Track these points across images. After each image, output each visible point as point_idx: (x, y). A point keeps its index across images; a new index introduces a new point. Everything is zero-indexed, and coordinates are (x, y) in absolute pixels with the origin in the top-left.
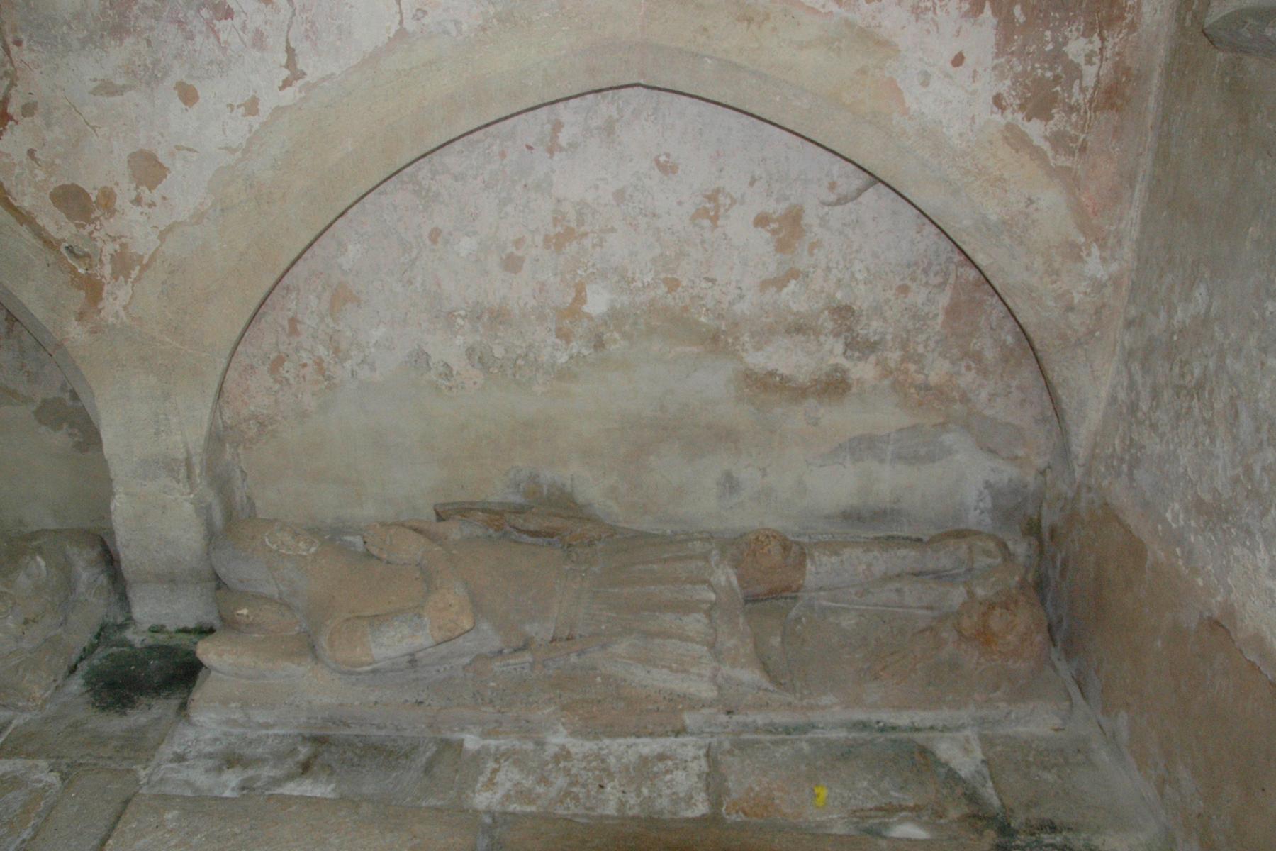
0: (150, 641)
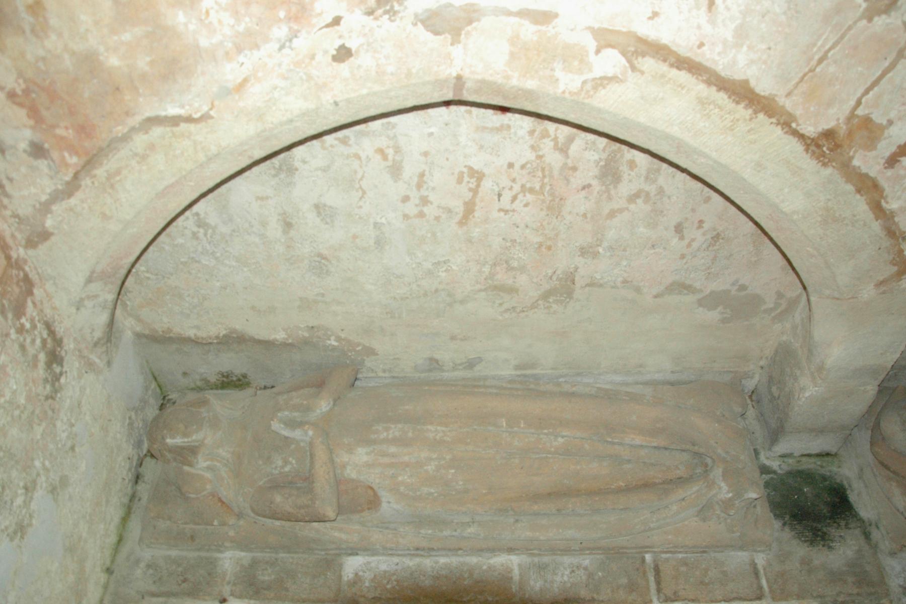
0: (786, 468)
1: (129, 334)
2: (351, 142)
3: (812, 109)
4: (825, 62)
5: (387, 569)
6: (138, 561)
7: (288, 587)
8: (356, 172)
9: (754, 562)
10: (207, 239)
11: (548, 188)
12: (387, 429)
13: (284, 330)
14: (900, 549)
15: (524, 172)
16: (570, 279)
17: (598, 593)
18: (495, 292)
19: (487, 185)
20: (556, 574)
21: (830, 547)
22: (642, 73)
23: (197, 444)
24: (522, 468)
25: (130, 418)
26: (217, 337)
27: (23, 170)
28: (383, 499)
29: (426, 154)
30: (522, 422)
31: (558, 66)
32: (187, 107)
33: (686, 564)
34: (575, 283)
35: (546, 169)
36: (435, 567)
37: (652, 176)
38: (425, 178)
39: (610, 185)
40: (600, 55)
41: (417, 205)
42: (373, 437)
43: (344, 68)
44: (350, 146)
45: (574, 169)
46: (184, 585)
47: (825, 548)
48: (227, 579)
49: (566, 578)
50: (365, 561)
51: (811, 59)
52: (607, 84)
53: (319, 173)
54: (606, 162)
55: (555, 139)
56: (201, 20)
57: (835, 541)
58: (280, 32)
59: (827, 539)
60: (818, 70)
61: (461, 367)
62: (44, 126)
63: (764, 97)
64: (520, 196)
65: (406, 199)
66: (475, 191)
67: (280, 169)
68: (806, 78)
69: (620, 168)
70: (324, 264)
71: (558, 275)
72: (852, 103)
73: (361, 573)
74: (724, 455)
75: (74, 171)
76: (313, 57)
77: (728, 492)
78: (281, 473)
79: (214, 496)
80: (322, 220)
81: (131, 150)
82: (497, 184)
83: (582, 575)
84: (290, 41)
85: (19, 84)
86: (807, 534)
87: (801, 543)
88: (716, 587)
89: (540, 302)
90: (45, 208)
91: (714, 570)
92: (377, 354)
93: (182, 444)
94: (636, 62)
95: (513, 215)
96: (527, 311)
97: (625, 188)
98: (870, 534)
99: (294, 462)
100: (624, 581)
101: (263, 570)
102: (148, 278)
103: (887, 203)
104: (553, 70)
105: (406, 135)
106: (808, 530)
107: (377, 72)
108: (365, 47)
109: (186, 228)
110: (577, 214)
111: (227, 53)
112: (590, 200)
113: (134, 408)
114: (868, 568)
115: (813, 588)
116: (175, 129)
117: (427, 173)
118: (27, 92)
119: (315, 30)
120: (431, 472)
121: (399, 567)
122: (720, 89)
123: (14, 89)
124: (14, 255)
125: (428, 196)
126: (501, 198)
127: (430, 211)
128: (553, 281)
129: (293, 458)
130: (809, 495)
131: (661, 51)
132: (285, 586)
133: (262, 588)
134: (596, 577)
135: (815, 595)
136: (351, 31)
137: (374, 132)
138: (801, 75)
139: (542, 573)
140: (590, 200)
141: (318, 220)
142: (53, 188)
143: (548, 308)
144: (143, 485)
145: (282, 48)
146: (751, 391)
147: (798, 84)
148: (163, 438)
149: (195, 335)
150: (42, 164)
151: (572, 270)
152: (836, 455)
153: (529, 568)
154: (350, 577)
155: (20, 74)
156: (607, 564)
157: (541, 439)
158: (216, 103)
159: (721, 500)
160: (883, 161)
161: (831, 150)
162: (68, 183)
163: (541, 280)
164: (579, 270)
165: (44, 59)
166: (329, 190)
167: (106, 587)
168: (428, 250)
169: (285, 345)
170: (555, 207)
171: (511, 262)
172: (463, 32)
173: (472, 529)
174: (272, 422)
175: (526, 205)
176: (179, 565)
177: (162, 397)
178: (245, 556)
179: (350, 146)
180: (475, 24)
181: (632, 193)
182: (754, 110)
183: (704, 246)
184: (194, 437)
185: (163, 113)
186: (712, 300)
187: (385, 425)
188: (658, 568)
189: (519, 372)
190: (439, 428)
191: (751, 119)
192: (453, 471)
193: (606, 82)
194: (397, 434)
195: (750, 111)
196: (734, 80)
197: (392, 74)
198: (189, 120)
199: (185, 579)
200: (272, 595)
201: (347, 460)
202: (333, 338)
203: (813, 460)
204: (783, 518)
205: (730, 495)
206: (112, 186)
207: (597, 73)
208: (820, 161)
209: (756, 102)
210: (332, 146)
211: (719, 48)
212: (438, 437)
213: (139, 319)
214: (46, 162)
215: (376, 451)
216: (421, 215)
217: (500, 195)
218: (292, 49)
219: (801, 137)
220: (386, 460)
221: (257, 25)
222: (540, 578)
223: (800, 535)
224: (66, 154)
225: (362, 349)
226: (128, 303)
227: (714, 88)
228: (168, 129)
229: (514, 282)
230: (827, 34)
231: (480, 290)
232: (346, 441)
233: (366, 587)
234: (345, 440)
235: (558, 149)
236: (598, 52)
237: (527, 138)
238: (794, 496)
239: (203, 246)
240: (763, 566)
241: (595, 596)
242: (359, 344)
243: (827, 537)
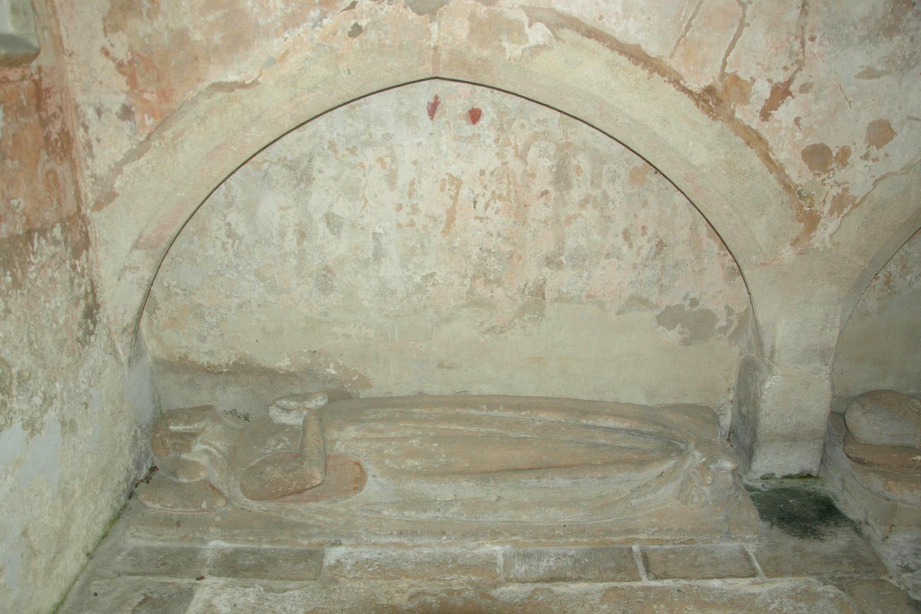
1: (149, 359)
2: (357, 152)
3: (692, 68)
4: (691, 29)
5: (369, 557)
8: (360, 180)
10: (234, 250)
11: (513, 194)
14: (889, 530)
15: (494, 178)
16: (539, 292)
18: (476, 308)
19: (465, 191)
22: (564, 41)
23: (196, 432)
26: (227, 365)
27: (111, 130)
28: (370, 473)
29: (415, 163)
31: (504, 37)
32: (243, 74)
34: (545, 298)
35: (510, 176)
37: (596, 181)
38: (415, 187)
39: (563, 191)
40: (532, 27)
41: (408, 214)
42: (362, 418)
43: (356, 42)
44: (357, 155)
45: (533, 175)
48: (208, 563)
51: (681, 27)
52: (540, 51)
53: (331, 181)
54: (557, 169)
55: (515, 147)
56: (262, 5)
58: (314, 14)
60: (687, 35)
62: (136, 92)
63: (654, 59)
64: (491, 203)
65: (399, 207)
66: (455, 198)
67: (301, 179)
68: (681, 42)
69: (570, 174)
70: (329, 279)
71: (530, 288)
72: (720, 63)
75: (149, 132)
76: (335, 34)
77: (702, 458)
80: (330, 230)
81: (195, 113)
82: (473, 191)
84: (321, 20)
85: (128, 56)
89: (516, 320)
90: (117, 169)
94: (557, 33)
95: (487, 223)
97: (576, 194)
98: (861, 530)
102: (177, 294)
103: (774, 155)
104: (501, 41)
105: (400, 145)
107: (379, 45)
108: (371, 25)
109: (217, 238)
110: (540, 221)
111: (277, 30)
112: (548, 207)
114: (863, 553)
116: (231, 94)
117: (416, 181)
118: (131, 62)
119: (338, 12)
121: (382, 556)
122: (622, 52)
123: (123, 61)
124: (83, 212)
125: (417, 204)
126: (476, 206)
127: (419, 219)
128: (526, 295)
131: (574, 24)
136: (362, 13)
137: (376, 142)
138: (676, 40)
140: (548, 207)
141: (327, 230)
142: (129, 147)
145: (315, 25)
147: (676, 47)
148: (167, 426)
150: (126, 125)
152: (817, 477)
153: (514, 556)
155: (131, 49)
158: (264, 71)
160: (758, 114)
161: (716, 105)
162: (141, 143)
163: (515, 294)
164: (547, 282)
165: (150, 36)
166: (338, 199)
167: (83, 568)
168: (417, 262)
170: (520, 212)
171: (488, 275)
172: (438, 12)
173: (455, 508)
175: (497, 213)
176: (160, 553)
179: (357, 155)
180: (445, 6)
181: (583, 198)
182: (650, 70)
183: (652, 254)
184: (196, 425)
185: (224, 80)
186: (669, 318)
191: (649, 78)
193: (539, 50)
195: (647, 71)
196: (629, 44)
197: (389, 46)
198: (243, 86)
201: (337, 437)
202: (332, 365)
203: (796, 481)
205: (704, 459)
206: (174, 147)
207: (532, 41)
208: (710, 115)
209: (649, 64)
210: (343, 156)
211: (614, 20)
214: (129, 123)
216: (412, 224)
217: (475, 203)
218: (321, 27)
219: (690, 93)
220: (373, 435)
221: (300, 8)
224: (146, 116)
225: (357, 379)
226: (155, 321)
227: (616, 53)
228: (226, 94)
229: (492, 296)
230: (686, 6)
235: (518, 156)
236: (530, 25)
237: (494, 146)
239: (229, 258)
240: (754, 553)
241: (582, 576)
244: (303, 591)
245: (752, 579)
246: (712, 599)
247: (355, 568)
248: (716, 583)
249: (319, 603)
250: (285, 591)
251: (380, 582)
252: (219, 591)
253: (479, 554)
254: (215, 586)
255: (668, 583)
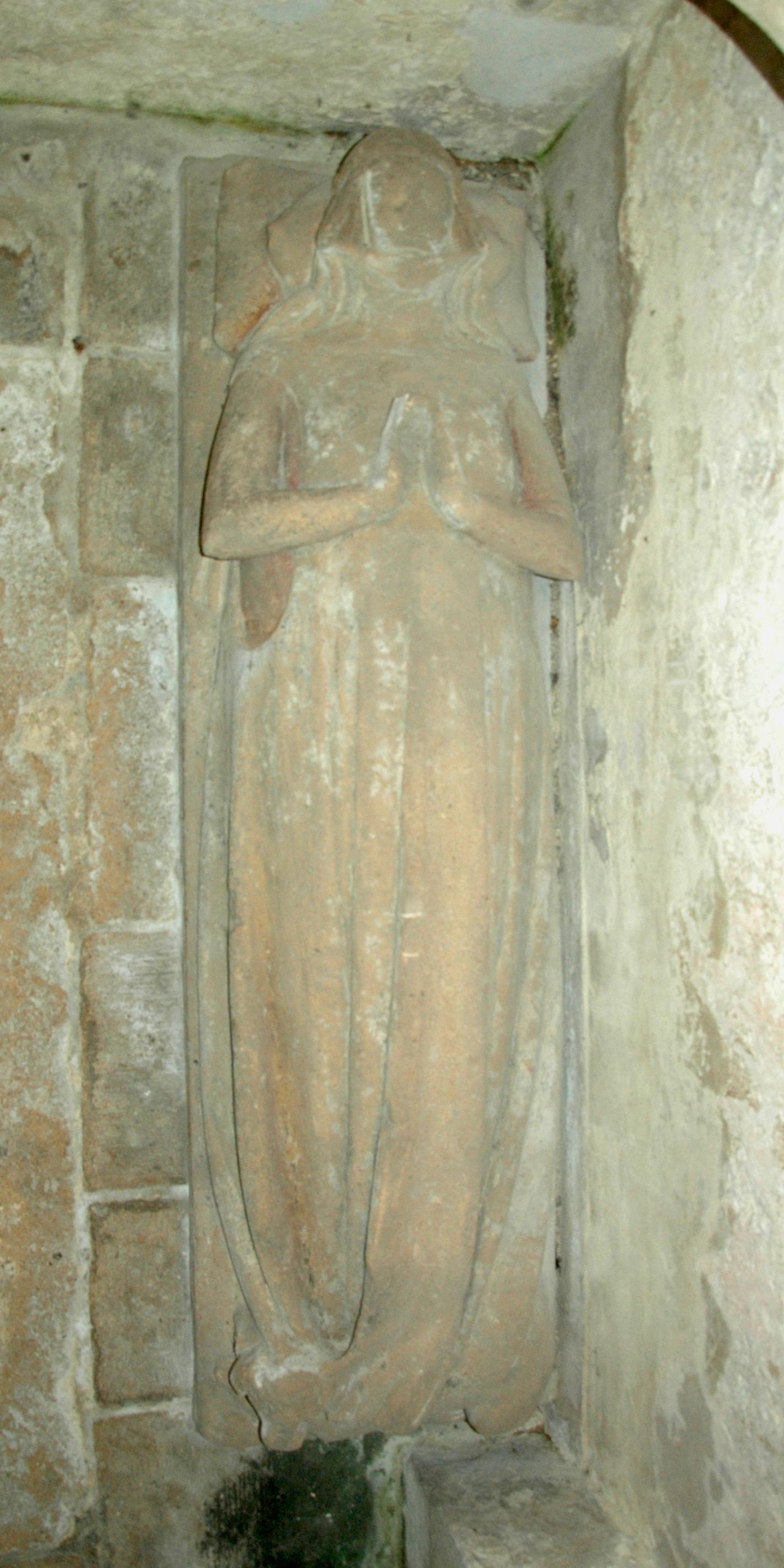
0: (378, 1482)
5: (152, 667)
6: (157, 163)
7: (111, 470)
9: (174, 1395)
12: (396, 654)
13: (644, 402)
17: (107, 1087)
20: (146, 1007)
21: (204, 1546)
23: (366, 238)
24: (317, 950)
25: (446, 89)
28: (256, 654)
30: (416, 955)
33: (169, 1263)
36: (159, 764)
42: (379, 625)
46: (110, 263)
47: (203, 1537)
49: (138, 1025)
50: (167, 622)
57: (219, 1558)
59: (223, 1543)
61: (593, 812)
70: (762, 479)
73: (142, 614)
74: (354, 1379)
78: (305, 428)
79: (272, 294)
83: (145, 1058)
86: (233, 1507)
87: (213, 1491)
88: (122, 1317)
89: (696, 1008)
91: (158, 1318)
92: (609, 623)
93: (363, 208)
96: (682, 973)
99: (325, 454)
100: (134, 1140)
101: (145, 418)
106: (241, 1508)
113: (472, 94)
115: (122, 1502)
120: (305, 754)
121: (156, 692)
129: (332, 453)
130: (317, 1521)
132: (112, 465)
133: (106, 419)
134: (140, 1086)
135: (107, 1502)
139: (148, 979)
143: (688, 1023)
144: (327, 149)
146: (550, 1434)
149: (630, 199)
151: (752, 1095)
153: (159, 954)
154: (134, 593)
156: (169, 1109)
157: (382, 995)
159: (253, 1362)
164: (751, 1110)
167: (101, 108)
169: (620, 407)
174: (407, 396)
176: (151, 247)
177: (530, 158)
178: (168, 381)
187: (406, 649)
188: (160, 1208)
189: (585, 941)
190: (400, 769)
192: (309, 802)
194: (386, 677)
199: (123, 263)
200: (93, 441)
201: (329, 570)
203: (395, 1539)
204: (267, 1463)
205: (259, 1384)
212: (377, 768)
213: (652, 53)
215: (345, 632)
220: (327, 654)
222: (137, 975)
223: (231, 1493)
231: (717, 867)
232: (369, 565)
233: (115, 626)
234: (373, 562)
238: (314, 1491)
240: (166, 1413)
241: (101, 1082)
242: (624, 581)
243: (225, 1543)
244: (51, 549)
245: (91, 1393)
246: (34, 1312)
247: (119, 641)
248: (82, 1326)
249: (18, 585)
250: (51, 515)
251: (82, 695)
252: (40, 391)
253: (165, 885)
254: (55, 378)
255: (84, 1240)
